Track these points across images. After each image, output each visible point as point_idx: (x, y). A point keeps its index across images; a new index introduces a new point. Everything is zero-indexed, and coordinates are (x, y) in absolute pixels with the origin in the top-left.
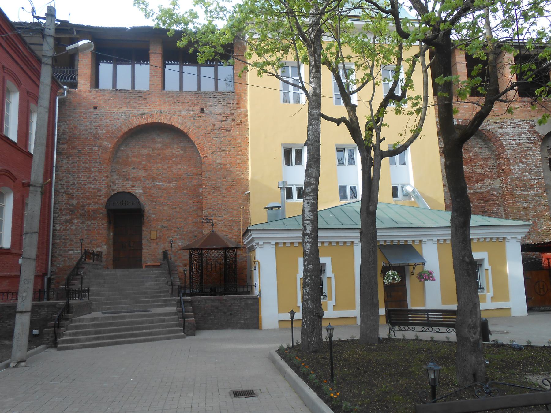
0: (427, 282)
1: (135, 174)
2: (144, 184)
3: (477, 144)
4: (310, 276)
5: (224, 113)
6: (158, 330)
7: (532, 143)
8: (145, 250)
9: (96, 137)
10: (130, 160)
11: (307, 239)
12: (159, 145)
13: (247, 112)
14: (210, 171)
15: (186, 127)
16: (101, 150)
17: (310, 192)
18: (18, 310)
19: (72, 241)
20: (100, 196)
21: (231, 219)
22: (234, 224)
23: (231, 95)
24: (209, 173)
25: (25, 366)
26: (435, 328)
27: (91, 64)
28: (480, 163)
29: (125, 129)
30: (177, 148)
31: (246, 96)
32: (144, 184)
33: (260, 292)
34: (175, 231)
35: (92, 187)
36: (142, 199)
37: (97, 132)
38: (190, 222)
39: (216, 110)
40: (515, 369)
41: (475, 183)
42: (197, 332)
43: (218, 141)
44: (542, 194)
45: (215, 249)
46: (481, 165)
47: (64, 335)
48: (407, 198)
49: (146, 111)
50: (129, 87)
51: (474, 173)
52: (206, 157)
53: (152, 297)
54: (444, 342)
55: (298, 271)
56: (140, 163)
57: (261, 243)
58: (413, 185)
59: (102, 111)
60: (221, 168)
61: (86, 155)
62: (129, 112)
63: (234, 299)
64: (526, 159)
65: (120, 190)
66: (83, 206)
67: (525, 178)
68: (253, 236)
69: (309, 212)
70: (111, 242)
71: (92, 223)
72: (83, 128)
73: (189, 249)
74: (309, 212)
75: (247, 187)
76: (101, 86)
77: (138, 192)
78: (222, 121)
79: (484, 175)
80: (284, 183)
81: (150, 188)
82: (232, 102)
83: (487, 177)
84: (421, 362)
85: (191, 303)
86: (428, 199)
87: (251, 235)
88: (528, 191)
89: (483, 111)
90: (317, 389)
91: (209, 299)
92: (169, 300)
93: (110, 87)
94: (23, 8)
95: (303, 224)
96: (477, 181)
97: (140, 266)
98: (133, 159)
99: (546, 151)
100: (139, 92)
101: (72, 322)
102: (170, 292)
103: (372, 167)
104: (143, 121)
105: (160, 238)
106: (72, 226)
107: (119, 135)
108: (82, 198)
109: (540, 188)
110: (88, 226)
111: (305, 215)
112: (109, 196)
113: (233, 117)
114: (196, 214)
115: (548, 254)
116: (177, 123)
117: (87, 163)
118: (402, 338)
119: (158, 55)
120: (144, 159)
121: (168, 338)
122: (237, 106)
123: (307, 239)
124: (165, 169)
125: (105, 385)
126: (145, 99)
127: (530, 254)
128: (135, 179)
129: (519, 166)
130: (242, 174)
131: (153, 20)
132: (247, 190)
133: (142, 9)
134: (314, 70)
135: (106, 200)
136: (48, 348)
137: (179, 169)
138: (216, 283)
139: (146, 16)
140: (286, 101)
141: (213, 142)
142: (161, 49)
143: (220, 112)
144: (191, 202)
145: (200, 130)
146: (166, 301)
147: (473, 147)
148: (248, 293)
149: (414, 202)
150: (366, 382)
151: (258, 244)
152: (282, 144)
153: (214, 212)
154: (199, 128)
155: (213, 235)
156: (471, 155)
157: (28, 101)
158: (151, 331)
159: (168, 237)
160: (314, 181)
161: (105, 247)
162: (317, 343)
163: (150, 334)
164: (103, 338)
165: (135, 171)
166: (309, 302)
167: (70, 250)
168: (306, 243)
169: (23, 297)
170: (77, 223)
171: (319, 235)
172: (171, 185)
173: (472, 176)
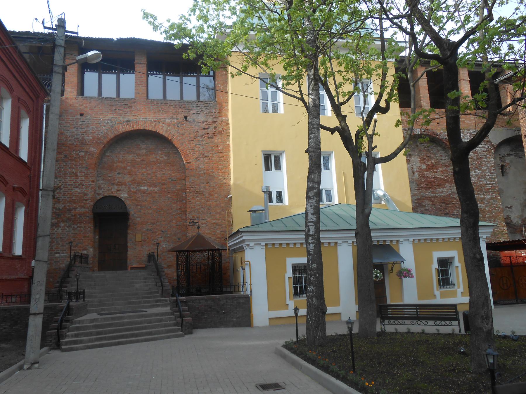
0: (405, 280)
1: (121, 179)
2: (129, 188)
3: (438, 151)
4: (315, 275)
5: (206, 121)
6: (157, 329)
7: (486, 151)
8: (130, 253)
9: (83, 143)
10: (115, 165)
11: (310, 240)
12: (144, 151)
13: (228, 120)
14: (194, 176)
15: (170, 134)
16: (87, 156)
17: (313, 196)
18: (31, 312)
19: (58, 244)
20: (86, 200)
21: (214, 221)
22: (217, 227)
23: (214, 104)
24: (192, 178)
25: (39, 368)
26: (423, 321)
27: (78, 73)
28: (441, 169)
29: (111, 136)
30: (161, 154)
31: (227, 106)
32: (129, 188)
33: (251, 291)
34: (160, 234)
35: (79, 191)
36: (127, 202)
37: (83, 138)
38: (174, 225)
39: (199, 118)
40: (514, 356)
41: (437, 187)
42: (194, 330)
43: (201, 148)
44: (496, 197)
45: (199, 251)
46: (442, 171)
47: (66, 336)
48: (377, 201)
49: (132, 118)
50: (114, 95)
51: (436, 178)
52: (190, 162)
53: (143, 298)
54: (435, 334)
55: (286, 270)
56: (125, 168)
57: (251, 244)
58: (383, 189)
59: (88, 117)
60: (204, 173)
61: (72, 160)
62: (115, 119)
63: (227, 298)
64: (482, 166)
65: (106, 194)
66: (70, 210)
67: (481, 183)
68: (244, 238)
69: (312, 214)
70: (97, 245)
71: (78, 227)
72: (70, 134)
73: (176, 251)
74: (312, 214)
75: (229, 191)
76: (86, 94)
77: (123, 195)
78: (204, 129)
79: (445, 180)
80: (267, 187)
81: (135, 192)
82: (214, 111)
83: (448, 182)
84: (426, 352)
85: (185, 303)
86: (397, 203)
87: (242, 236)
88: (484, 195)
89: (488, 122)
90: (343, 379)
91: (202, 299)
92: (160, 301)
93: (95, 94)
94: (36, 19)
95: (306, 226)
96: (439, 186)
97: (126, 268)
98: (118, 164)
99: (498, 158)
100: (125, 100)
101: (72, 323)
102: (160, 292)
103: (366, 173)
104: (129, 128)
105: (145, 241)
106: (58, 229)
107: (106, 141)
108: (69, 202)
109: (494, 192)
110: (74, 229)
111: (309, 217)
112: (95, 201)
113: (215, 125)
114: (180, 217)
115: (506, 252)
116: (162, 130)
117: (73, 168)
118: (394, 331)
119: (143, 65)
120: (129, 164)
121: (168, 337)
122: (219, 114)
123: (310, 240)
124: (149, 174)
125: (130, 383)
126: (131, 107)
127: (494, 252)
128: (120, 184)
129: (475, 172)
130: (224, 179)
131: (161, 33)
132: (229, 194)
133: (150, 22)
134: (313, 83)
135: (92, 204)
136: (51, 349)
137: (163, 174)
138: (204, 285)
139: (154, 29)
140: (266, 110)
141: (196, 149)
142: (146, 60)
143: (203, 120)
144: (175, 205)
145: (184, 136)
146: (157, 301)
147: (435, 155)
148: (231, 292)
149: (385, 205)
150: (385, 372)
151: (248, 245)
152: (262, 151)
153: (198, 215)
154: (182, 135)
155: (199, 238)
156: (433, 162)
157: (19, 107)
158: (150, 330)
159: (152, 240)
160: (316, 186)
161: (91, 250)
162: (322, 337)
163: (150, 334)
164: (105, 339)
165: (120, 176)
166: (314, 299)
167: (56, 253)
168: (309, 244)
169: (36, 299)
170: (64, 227)
171: (321, 236)
172: (156, 189)
173: (434, 181)
